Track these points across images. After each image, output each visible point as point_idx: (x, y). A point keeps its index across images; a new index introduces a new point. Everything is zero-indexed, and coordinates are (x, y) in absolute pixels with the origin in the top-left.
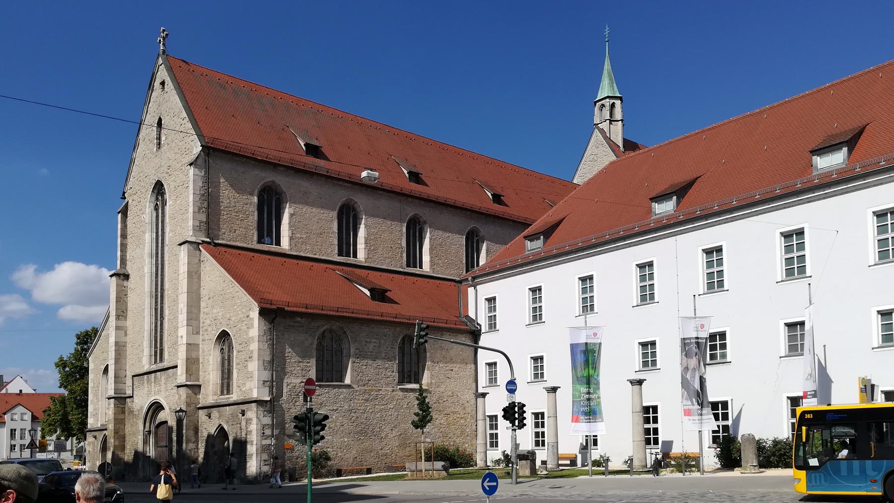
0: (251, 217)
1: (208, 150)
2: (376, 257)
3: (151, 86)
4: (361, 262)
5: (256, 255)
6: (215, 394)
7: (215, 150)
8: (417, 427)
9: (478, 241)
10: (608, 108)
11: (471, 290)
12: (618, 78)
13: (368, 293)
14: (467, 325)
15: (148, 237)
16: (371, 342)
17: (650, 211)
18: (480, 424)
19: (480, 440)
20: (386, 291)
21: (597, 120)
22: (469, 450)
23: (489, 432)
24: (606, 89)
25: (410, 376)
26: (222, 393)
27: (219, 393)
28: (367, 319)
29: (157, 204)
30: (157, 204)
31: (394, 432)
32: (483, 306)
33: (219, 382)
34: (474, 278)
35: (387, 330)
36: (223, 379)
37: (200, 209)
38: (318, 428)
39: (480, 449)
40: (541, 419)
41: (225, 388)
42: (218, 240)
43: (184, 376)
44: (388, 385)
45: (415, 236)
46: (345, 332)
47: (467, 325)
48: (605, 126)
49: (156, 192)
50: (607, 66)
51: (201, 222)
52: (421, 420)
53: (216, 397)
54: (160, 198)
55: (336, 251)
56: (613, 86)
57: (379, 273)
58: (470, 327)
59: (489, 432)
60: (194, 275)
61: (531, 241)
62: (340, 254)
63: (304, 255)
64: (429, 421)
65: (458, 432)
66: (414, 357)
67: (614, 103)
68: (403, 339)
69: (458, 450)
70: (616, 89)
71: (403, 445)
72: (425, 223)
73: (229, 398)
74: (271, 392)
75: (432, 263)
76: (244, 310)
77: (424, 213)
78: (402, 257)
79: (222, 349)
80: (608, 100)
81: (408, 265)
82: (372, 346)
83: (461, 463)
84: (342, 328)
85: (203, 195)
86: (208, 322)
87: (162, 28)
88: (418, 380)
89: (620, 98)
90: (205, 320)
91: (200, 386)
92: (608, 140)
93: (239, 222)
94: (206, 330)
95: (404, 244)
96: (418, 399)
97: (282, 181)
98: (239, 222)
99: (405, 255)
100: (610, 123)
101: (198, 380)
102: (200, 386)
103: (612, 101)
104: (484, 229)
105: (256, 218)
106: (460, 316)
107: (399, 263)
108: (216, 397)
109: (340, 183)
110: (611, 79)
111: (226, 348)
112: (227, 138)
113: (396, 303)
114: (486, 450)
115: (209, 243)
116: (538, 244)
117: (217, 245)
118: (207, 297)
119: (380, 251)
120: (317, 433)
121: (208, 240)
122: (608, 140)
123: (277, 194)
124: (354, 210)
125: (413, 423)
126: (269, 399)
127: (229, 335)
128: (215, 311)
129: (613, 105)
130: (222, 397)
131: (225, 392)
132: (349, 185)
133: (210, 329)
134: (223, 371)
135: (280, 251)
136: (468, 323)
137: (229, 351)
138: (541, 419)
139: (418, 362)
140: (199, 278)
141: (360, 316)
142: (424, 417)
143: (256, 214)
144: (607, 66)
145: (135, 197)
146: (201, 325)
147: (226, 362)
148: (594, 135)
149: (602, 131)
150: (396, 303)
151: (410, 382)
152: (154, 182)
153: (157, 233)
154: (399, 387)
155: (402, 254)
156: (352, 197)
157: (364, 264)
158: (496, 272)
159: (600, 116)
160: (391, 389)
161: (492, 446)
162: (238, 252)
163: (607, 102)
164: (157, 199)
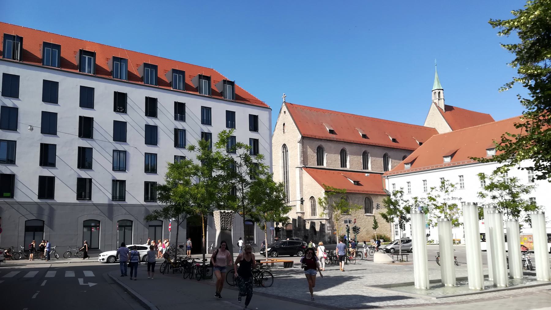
0: (315, 157)
1: (303, 138)
2: (353, 167)
3: (280, 112)
4: (348, 169)
5: (318, 170)
6: (310, 216)
7: (305, 137)
8: (374, 229)
9: (387, 157)
10: (437, 94)
11: (386, 180)
12: (440, 81)
13: (353, 183)
14: (386, 193)
15: (281, 162)
16: (356, 200)
17: (443, 161)
18: (392, 228)
19: (392, 233)
20: (359, 182)
21: (433, 98)
22: (389, 236)
23: (395, 230)
24: (436, 86)
25: (368, 211)
26: (312, 215)
27: (311, 215)
28: (354, 193)
29: (283, 151)
30: (283, 151)
31: (364, 229)
32: (391, 186)
33: (311, 212)
34: (388, 176)
35: (360, 196)
36: (312, 211)
37: (301, 156)
38: (358, 230)
39: (392, 236)
40: (462, 186)
41: (313, 214)
42: (308, 165)
43: (300, 209)
44: (362, 214)
45: (365, 158)
46: (348, 197)
47: (386, 193)
48: (436, 101)
49: (283, 147)
50: (436, 76)
51: (302, 160)
52: (375, 227)
53: (310, 217)
54: (285, 149)
55: (340, 166)
56: (439, 85)
57: (354, 173)
58: (387, 194)
59: (395, 230)
60: (301, 178)
61: (407, 165)
62: (341, 167)
63: (331, 168)
64: (377, 227)
65: (385, 230)
66: (369, 204)
67: (440, 92)
68: (366, 198)
69: (385, 236)
70: (440, 86)
71: (367, 234)
72: (369, 153)
73: (315, 217)
74: (329, 216)
75: (372, 168)
76: (320, 191)
77: (368, 149)
78: (361, 166)
79: (311, 202)
80: (437, 90)
81: (364, 169)
82: (356, 201)
83: (386, 241)
84: (347, 196)
85: (302, 152)
86: (306, 193)
87: (284, 94)
88: (371, 213)
89: (443, 90)
90: (305, 192)
91: (304, 213)
92: (438, 107)
93: (312, 159)
94: (306, 195)
95: (362, 162)
96: (374, 220)
97: (323, 144)
98: (312, 159)
99: (362, 165)
100: (439, 100)
101: (303, 211)
102: (304, 213)
103: (439, 91)
104: (390, 153)
105: (316, 157)
106: (383, 189)
107: (360, 168)
108: (310, 217)
109: (341, 142)
110: (438, 82)
111: (313, 201)
112: (310, 133)
113: (362, 185)
114: (395, 236)
115: (304, 167)
116: (409, 166)
117: (307, 167)
118: (306, 185)
119: (354, 165)
120: (358, 232)
121: (304, 166)
122: (438, 107)
123: (322, 148)
124: (345, 151)
125: (373, 228)
126: (329, 218)
127: (314, 197)
128: (309, 189)
129: (439, 93)
130: (312, 217)
131: (313, 215)
132: (343, 143)
133: (307, 195)
134: (312, 209)
135: (324, 168)
136: (387, 192)
137: (314, 202)
138: (462, 186)
139: (371, 206)
140: (302, 178)
141: (353, 192)
142: (376, 226)
143: (316, 156)
144: (436, 76)
145: (275, 147)
146: (304, 193)
147: (313, 206)
148: (432, 105)
149: (435, 104)
150: (362, 185)
151: (368, 213)
152: (283, 144)
153: (284, 160)
154: (365, 215)
155: (361, 165)
156: (344, 147)
157: (349, 170)
158: (396, 174)
159: (434, 98)
160: (363, 215)
161: (396, 235)
162: (313, 169)
163: (437, 91)
164: (283, 149)
